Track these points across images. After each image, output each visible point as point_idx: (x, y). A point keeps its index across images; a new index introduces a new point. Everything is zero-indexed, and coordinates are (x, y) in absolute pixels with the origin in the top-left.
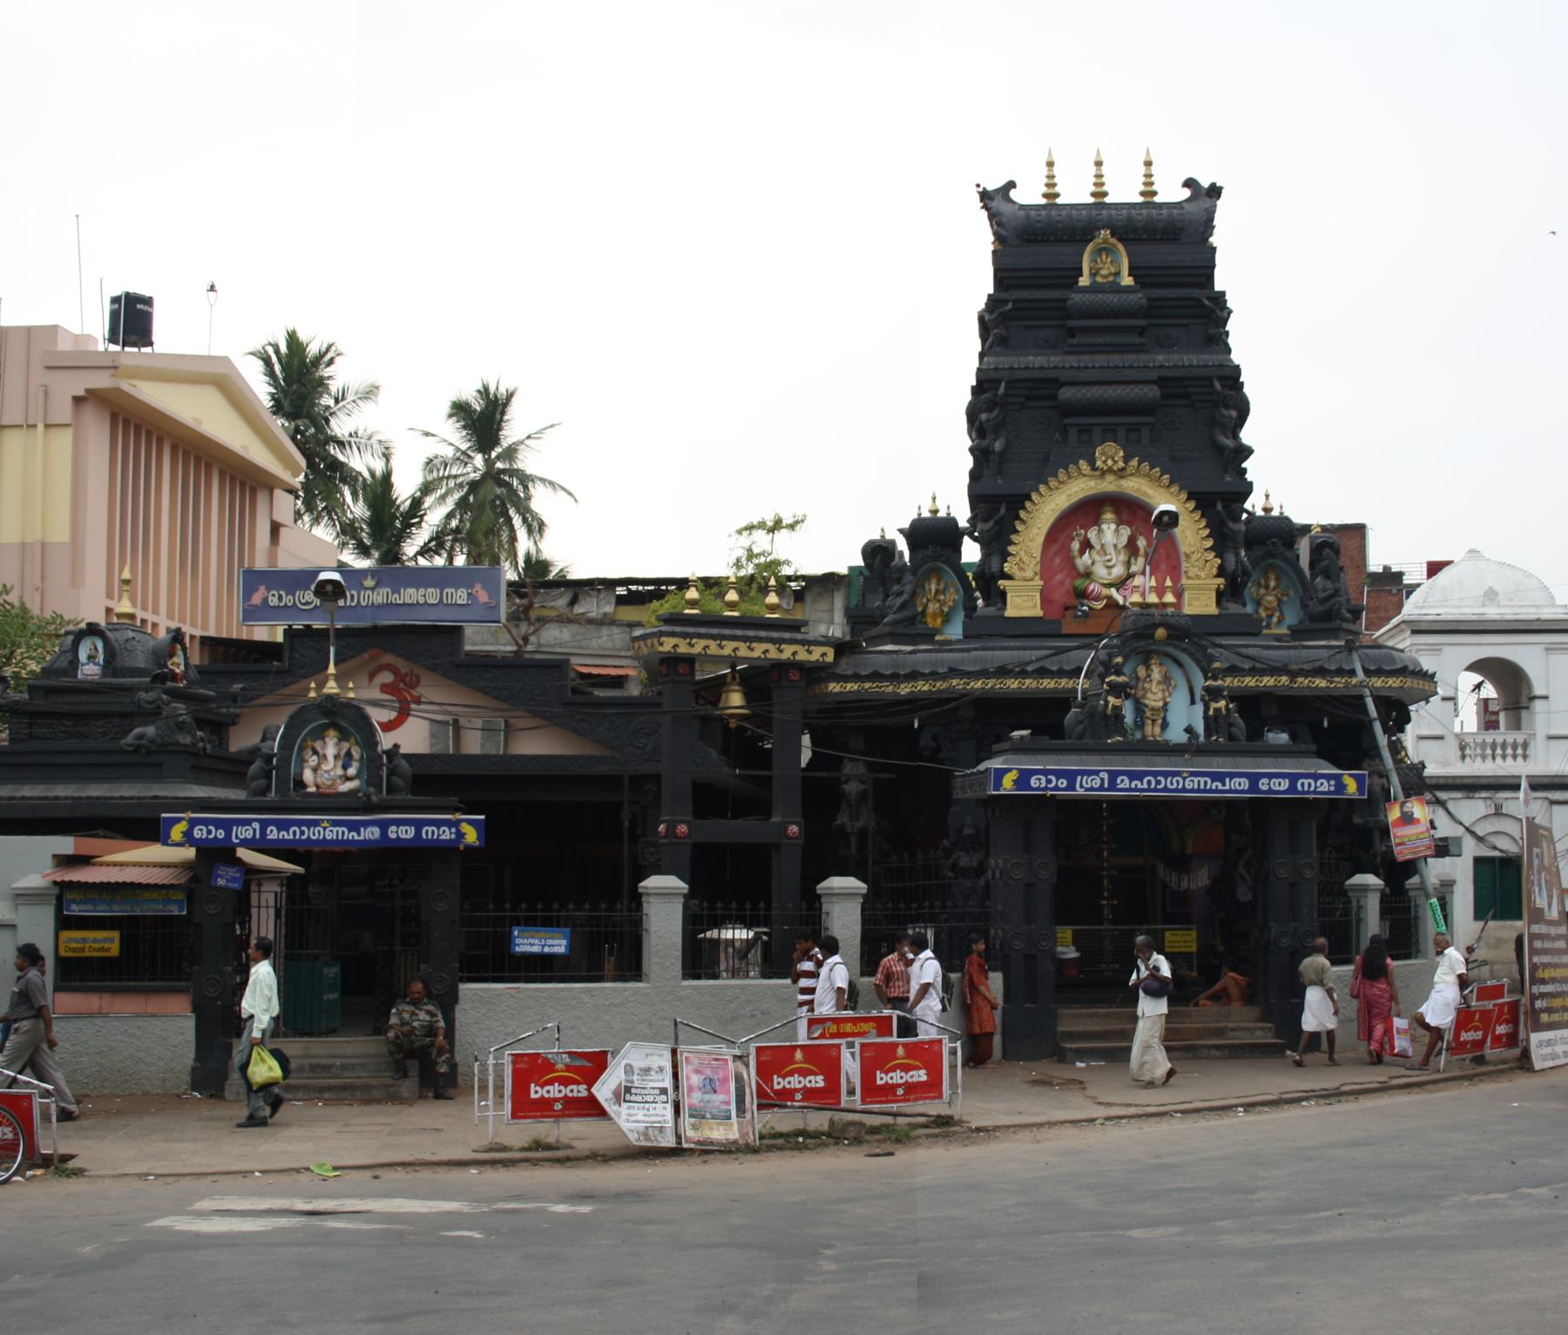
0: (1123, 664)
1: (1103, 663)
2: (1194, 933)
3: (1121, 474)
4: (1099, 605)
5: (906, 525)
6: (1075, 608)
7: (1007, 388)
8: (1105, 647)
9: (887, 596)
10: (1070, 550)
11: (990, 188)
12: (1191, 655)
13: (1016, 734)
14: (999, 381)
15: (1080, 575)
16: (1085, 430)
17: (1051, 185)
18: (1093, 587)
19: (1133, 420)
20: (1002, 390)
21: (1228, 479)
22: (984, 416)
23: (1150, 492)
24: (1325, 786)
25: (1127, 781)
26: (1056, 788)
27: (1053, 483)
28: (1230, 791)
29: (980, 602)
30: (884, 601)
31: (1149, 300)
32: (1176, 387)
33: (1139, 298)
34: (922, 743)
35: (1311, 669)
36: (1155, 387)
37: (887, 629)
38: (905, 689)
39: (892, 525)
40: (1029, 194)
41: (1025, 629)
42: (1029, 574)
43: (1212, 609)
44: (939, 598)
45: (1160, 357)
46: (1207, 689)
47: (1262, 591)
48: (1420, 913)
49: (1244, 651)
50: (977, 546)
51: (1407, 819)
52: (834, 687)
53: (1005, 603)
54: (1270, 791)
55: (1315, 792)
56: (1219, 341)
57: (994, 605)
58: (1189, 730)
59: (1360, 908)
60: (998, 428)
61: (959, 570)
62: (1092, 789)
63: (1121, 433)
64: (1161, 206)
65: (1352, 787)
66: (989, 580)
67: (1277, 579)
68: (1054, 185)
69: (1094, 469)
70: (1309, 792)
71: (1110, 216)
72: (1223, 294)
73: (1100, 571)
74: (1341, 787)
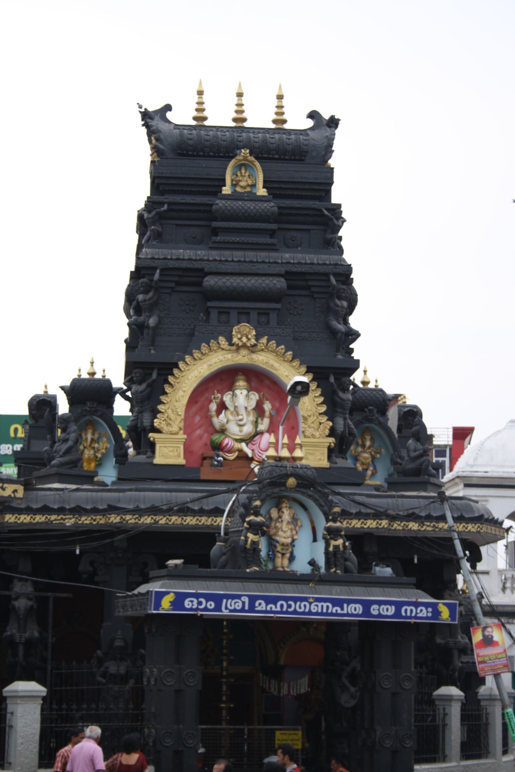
0: (261, 506)
1: (244, 506)
2: (300, 733)
3: (253, 349)
4: (231, 457)
5: (67, 383)
6: (212, 458)
7: (161, 275)
8: (244, 492)
9: (54, 442)
10: (208, 410)
11: (151, 109)
12: (316, 501)
13: (171, 562)
14: (155, 269)
15: (216, 431)
16: (224, 312)
17: (200, 110)
18: (228, 442)
19: (263, 305)
20: (157, 276)
21: (340, 357)
22: (140, 297)
23: (276, 365)
24: (424, 613)
25: (263, 604)
26: (206, 609)
27: (197, 354)
28: (348, 615)
29: (131, 451)
30: (52, 446)
31: (279, 208)
32: (299, 280)
33: (271, 206)
34: (81, 568)
35: (401, 515)
36: (282, 280)
37: (54, 470)
38: (70, 521)
39: (54, 382)
40: (182, 116)
41: (171, 475)
42: (175, 429)
43: (325, 463)
44: (95, 446)
45: (287, 255)
46: (329, 530)
47: (360, 449)
48: (490, 721)
49: (357, 498)
50: (127, 405)
51: (488, 641)
52: (10, 518)
53: (153, 452)
54: (380, 615)
55: (416, 617)
56: (334, 245)
57: (145, 453)
58: (312, 563)
59: (445, 714)
60: (153, 306)
61: (112, 423)
62: (235, 610)
63: (254, 315)
64: (290, 132)
65: (445, 613)
66: (141, 433)
67: (372, 439)
68: (203, 110)
69: (231, 344)
70: (411, 617)
71: (249, 138)
72: (339, 206)
73: (233, 429)
74: (437, 613)
